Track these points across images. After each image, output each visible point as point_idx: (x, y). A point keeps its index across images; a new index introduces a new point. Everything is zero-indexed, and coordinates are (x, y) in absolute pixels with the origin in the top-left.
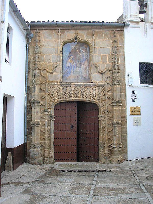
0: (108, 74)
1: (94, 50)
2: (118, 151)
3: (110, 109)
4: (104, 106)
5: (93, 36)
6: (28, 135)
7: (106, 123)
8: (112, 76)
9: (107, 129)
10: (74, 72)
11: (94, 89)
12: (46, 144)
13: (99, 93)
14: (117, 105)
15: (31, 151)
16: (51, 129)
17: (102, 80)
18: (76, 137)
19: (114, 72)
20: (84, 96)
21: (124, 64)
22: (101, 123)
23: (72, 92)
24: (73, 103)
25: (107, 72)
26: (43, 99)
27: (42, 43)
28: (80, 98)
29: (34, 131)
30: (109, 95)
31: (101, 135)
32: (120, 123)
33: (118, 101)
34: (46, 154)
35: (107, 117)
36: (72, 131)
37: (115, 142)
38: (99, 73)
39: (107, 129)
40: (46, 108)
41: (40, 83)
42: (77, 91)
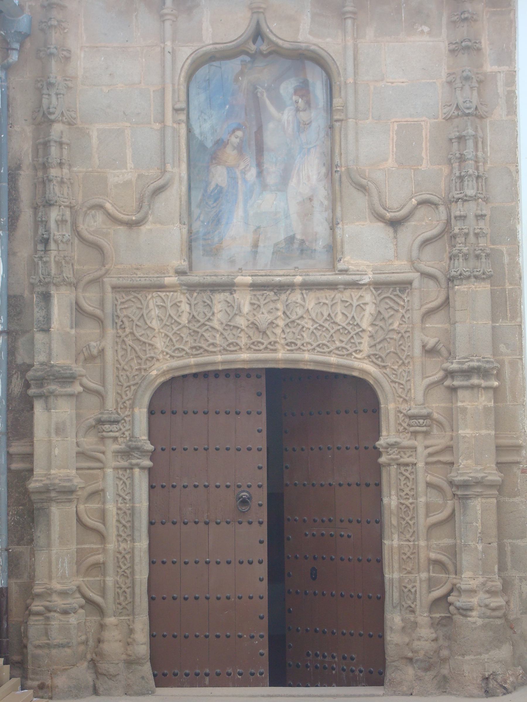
0: (428, 224)
1: (351, 99)
2: (484, 627)
3: (436, 406)
4: (405, 395)
5: (349, 22)
6: (19, 549)
7: (415, 481)
8: (447, 233)
9: (422, 511)
10: (251, 213)
11: (355, 304)
12: (110, 595)
13: (381, 324)
14: (472, 387)
15: (32, 632)
16: (132, 515)
17: (397, 257)
18: (262, 552)
19: (458, 213)
20: (299, 343)
21: (512, 169)
22: (390, 478)
23: (241, 321)
24: (249, 376)
25: (423, 211)
26: (91, 358)
27: (82, 63)
28: (280, 355)
29: (49, 530)
30: (432, 333)
31: (392, 542)
32: (490, 478)
33: (475, 364)
34: (113, 645)
35: (420, 449)
36: (245, 524)
37: (469, 579)
38: (380, 218)
39: (422, 511)
40: (110, 404)
41: (73, 280)
42: (263, 318)
